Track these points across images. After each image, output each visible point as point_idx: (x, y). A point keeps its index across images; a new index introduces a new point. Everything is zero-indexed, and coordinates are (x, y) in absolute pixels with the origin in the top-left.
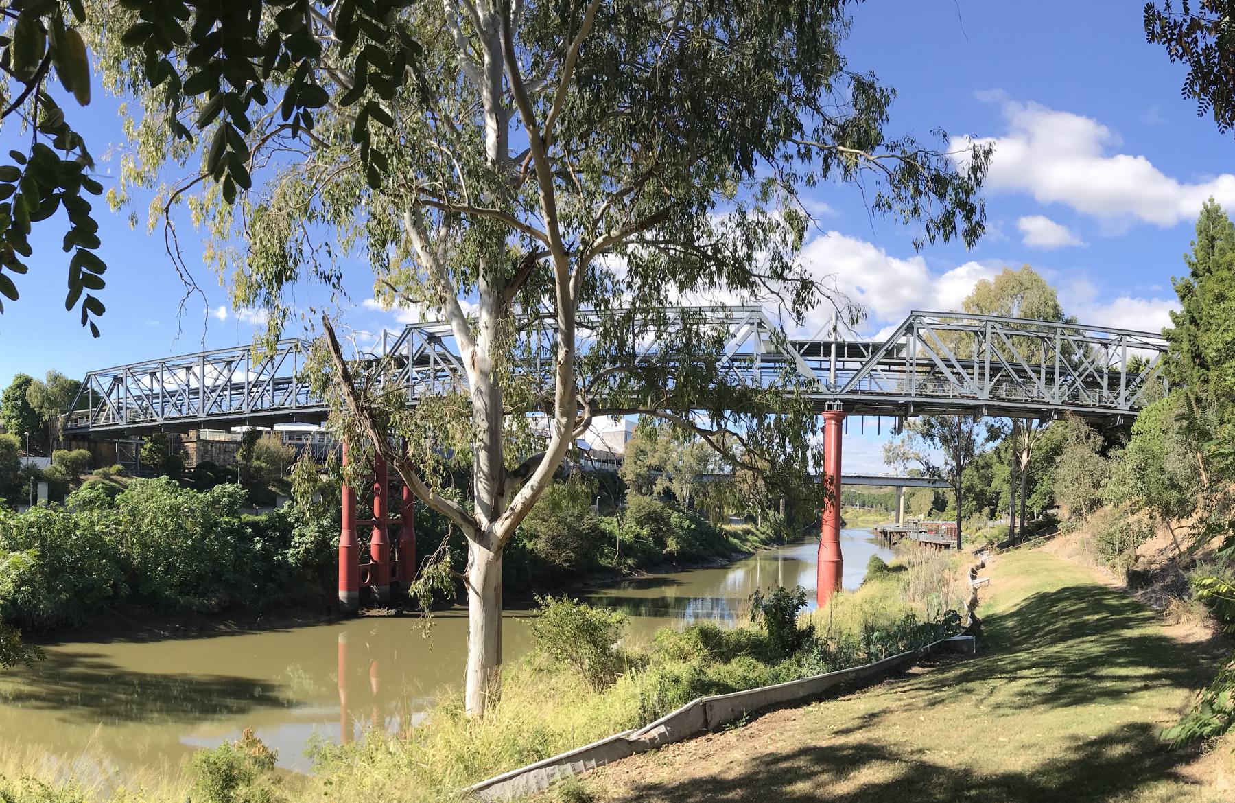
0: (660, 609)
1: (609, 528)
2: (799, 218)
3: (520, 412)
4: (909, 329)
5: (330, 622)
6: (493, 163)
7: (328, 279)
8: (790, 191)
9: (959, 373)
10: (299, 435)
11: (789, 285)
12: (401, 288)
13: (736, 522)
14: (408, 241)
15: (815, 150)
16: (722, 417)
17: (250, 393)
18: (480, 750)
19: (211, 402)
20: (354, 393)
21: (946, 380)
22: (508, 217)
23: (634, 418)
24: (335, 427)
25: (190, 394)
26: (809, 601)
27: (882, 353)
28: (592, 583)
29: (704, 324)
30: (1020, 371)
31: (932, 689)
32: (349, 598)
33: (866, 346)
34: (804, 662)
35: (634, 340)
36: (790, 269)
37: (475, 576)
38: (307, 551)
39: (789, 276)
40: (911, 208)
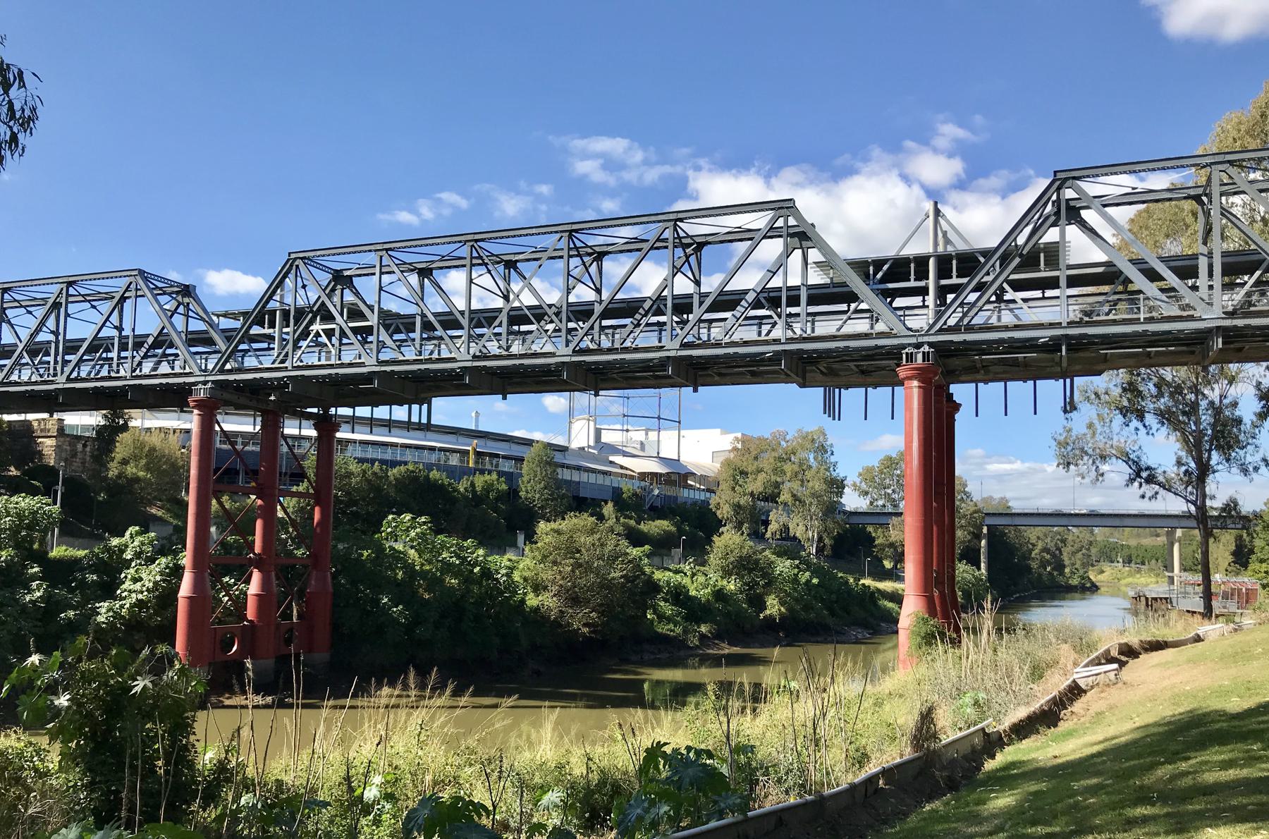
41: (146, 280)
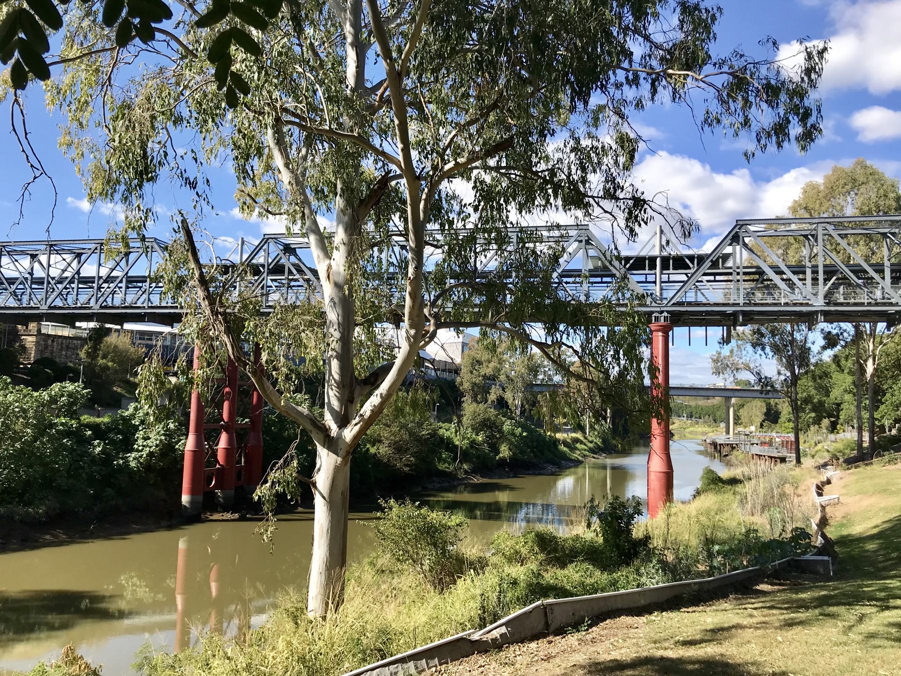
0: (494, 513)
1: (447, 434)
2: (630, 140)
3: (369, 324)
4: (735, 238)
5: (170, 528)
6: (353, 90)
7: (193, 185)
8: (622, 116)
9: (790, 280)
10: (150, 334)
11: (621, 203)
12: (261, 199)
13: (566, 431)
14: (270, 157)
15: (642, 75)
16: (557, 329)
17: (99, 288)
18: (323, 651)
19: (55, 294)
20: (211, 298)
21: (776, 286)
22: (364, 143)
23: (475, 332)
24: (189, 328)
25: (32, 283)
26: (644, 510)
27: (708, 263)
28: (430, 486)
29: (542, 242)
30: (858, 271)
31: (786, 609)
32: (192, 502)
33: (691, 258)
34: (642, 570)
35: (476, 257)
36: (622, 189)
37: (322, 479)
38: (151, 454)
39: (622, 196)
40: (741, 119)
41: (158, 243)
